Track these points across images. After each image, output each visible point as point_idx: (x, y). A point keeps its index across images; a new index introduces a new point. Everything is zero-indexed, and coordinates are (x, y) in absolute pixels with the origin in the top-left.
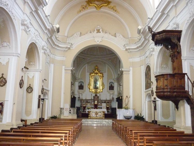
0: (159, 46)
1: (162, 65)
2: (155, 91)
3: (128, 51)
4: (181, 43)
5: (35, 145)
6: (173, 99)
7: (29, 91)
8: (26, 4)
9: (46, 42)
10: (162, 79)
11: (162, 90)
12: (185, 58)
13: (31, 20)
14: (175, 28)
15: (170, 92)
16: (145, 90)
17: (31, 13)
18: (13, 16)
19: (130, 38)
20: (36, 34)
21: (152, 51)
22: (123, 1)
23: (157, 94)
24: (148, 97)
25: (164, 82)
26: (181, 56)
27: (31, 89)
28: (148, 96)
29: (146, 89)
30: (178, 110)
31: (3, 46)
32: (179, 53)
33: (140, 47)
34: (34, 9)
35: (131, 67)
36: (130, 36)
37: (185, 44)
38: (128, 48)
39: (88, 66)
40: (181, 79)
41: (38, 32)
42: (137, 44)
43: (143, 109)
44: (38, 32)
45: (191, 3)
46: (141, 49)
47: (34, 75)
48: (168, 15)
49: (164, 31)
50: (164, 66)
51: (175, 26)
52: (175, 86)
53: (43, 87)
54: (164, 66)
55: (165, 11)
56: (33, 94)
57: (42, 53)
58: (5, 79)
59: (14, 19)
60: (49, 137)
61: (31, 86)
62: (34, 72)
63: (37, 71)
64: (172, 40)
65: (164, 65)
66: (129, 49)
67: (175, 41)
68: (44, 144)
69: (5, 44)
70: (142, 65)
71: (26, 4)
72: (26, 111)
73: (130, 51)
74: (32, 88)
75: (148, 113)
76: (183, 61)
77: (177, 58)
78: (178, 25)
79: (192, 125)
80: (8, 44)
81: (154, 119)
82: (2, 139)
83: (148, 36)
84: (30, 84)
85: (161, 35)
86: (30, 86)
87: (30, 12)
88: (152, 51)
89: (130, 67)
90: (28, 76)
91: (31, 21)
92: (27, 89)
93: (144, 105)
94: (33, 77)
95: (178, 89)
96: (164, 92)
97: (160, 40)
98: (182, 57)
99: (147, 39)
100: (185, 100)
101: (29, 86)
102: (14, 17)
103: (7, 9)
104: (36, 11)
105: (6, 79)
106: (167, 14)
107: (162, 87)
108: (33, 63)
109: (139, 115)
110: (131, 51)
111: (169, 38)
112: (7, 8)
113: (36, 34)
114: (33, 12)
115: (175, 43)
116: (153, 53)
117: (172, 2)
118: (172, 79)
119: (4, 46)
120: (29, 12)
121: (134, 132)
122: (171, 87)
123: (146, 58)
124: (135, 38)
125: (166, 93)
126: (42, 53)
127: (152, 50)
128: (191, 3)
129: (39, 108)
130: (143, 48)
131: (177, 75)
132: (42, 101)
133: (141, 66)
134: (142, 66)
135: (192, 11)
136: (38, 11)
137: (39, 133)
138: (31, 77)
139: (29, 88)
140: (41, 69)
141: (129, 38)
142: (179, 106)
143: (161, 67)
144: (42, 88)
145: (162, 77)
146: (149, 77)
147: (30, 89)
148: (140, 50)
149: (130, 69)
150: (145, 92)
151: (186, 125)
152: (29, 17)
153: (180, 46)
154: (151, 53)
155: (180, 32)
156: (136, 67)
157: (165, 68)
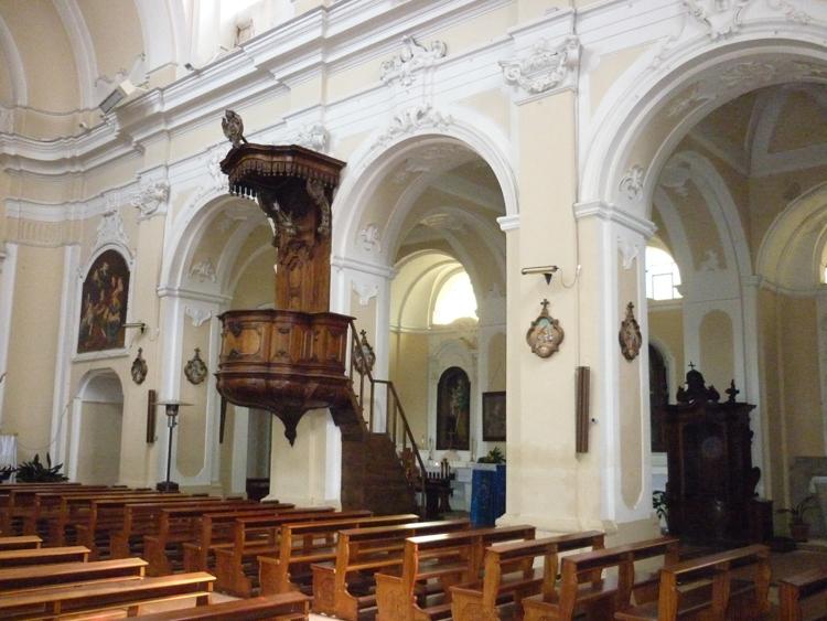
1: (194, 262)
2: (215, 372)
3: (12, 166)
4: (336, 208)
8: (418, 35)
10: (263, 328)
11: (263, 370)
12: (341, 263)
14: (319, 147)
15: (291, 377)
16: (74, 354)
19: (25, 108)
21: (160, 200)
24: (90, 383)
25: (274, 339)
26: (330, 252)
28: (88, 380)
29: (82, 347)
30: (292, 443)
32: (323, 240)
33: (73, 161)
35: (16, 243)
36: (23, 100)
37: (346, 211)
38: (13, 153)
40: (335, 336)
42: (64, 148)
43: (54, 435)
45: (408, 85)
46: (79, 172)
48: (282, 84)
49: (295, 151)
50: (202, 270)
51: (320, 139)
52: (314, 359)
53: (140, 355)
54: (202, 270)
55: (277, 69)
60: (19, 587)
64: (309, 185)
65: (203, 263)
66: (17, 158)
67: (316, 192)
68: (728, 547)
70: (71, 240)
73: (18, 169)
75: (79, 456)
76: (333, 270)
77: (311, 257)
78: (327, 138)
79: (342, 496)
81: (165, 480)
82: (9, 608)
83: (146, 130)
85: (275, 159)
88: (160, 200)
89: (5, 242)
93: (65, 421)
95: (324, 369)
96: (268, 376)
97: (267, 177)
98: (332, 256)
99: (135, 139)
100: (328, 410)
101: (191, 356)
106: (281, 80)
107: (263, 358)
109: (42, 461)
110: (21, 171)
115: (315, 200)
116: (162, 208)
117: (320, 50)
121: (293, 530)
122: (301, 361)
123: (103, 219)
124: (48, 113)
125: (277, 382)
127: (160, 193)
128: (408, 85)
129: (586, 450)
130: (84, 172)
131: (322, 321)
133: (63, 244)
134: (69, 249)
135: (408, 115)
137: (82, 561)
141: (21, 106)
142: (298, 429)
143: (191, 268)
144: (136, 357)
145: (269, 318)
146: (115, 301)
148: (67, 173)
149: (5, 252)
150: (75, 363)
151: (324, 496)
153: (330, 216)
154: (151, 206)
155: (338, 166)
156: (45, 247)
157: (202, 275)
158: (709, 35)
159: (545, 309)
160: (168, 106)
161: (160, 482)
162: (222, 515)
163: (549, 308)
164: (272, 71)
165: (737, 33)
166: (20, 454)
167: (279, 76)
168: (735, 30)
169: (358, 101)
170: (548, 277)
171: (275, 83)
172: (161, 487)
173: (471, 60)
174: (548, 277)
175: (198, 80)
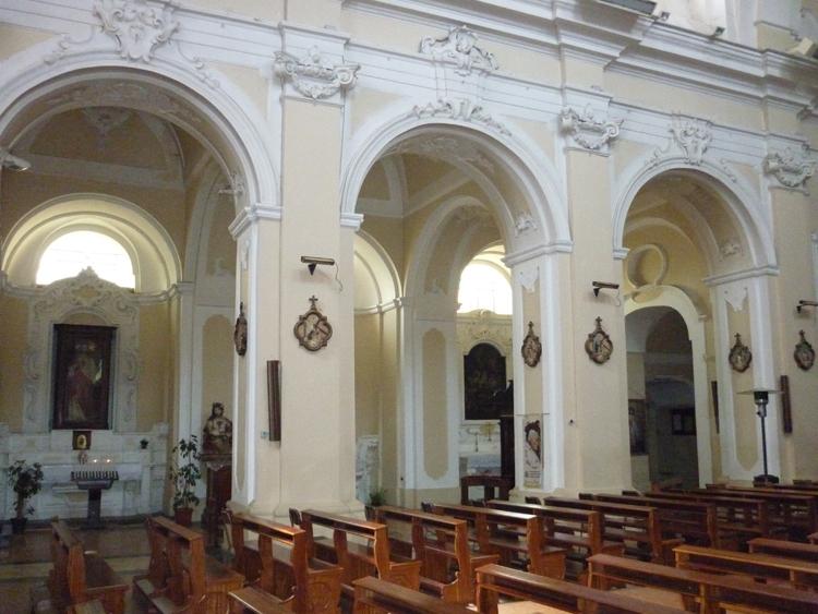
7: (740, 365)
8: (566, 52)
18: (493, 128)
20: (678, 132)
27: (743, 353)
31: (727, 256)
34: (614, 51)
41: (692, 118)
44: (692, 118)
47: (745, 292)
55: (565, 32)
56: (541, 369)
57: (772, 188)
58: (590, 336)
59: (503, 135)
62: (745, 283)
63: (537, 256)
69: (730, 249)
71: (566, 52)
72: (739, 448)
74: (746, 349)
80: (737, 245)
86: (531, 332)
90: (728, 303)
92: (731, 356)
94: (746, 301)
103: (456, 119)
104: (634, 48)
108: (737, 245)
112: (451, 117)
113: (678, 132)
118: (43, 583)
119: (730, 254)
126: (772, 188)
132: (759, 404)
138: (737, 306)
139: (738, 351)
140: (772, 260)
147: (740, 354)
152: (602, 93)
158: (119, 53)
159: (313, 304)
160: (646, 42)
161: (757, 475)
162: (677, 502)
163: (317, 304)
164: (562, 31)
165: (146, 63)
166: (124, 510)
167: (565, 40)
168: (147, 59)
169: (389, 59)
170: (312, 268)
171: (554, 42)
172: (759, 480)
173: (528, 88)
174: (312, 268)
175: (707, 45)
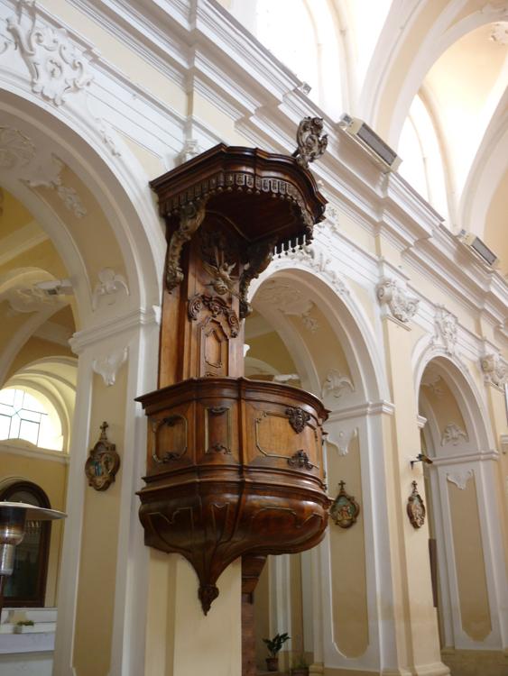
0: (290, 252)
5: (3, 589)
6: (186, 543)
7: (100, 481)
9: (474, 336)
13: (408, 279)
16: (141, 485)
17: (406, 252)
22: (379, 100)
23: (154, 505)
39: (197, 406)
61: (349, 491)
84: (342, 484)
87: (402, 253)
91: (409, 282)
102: (408, 285)
105: (118, 451)
111: (274, 196)
114: (411, 249)
120: (398, 253)
136: (430, 240)
